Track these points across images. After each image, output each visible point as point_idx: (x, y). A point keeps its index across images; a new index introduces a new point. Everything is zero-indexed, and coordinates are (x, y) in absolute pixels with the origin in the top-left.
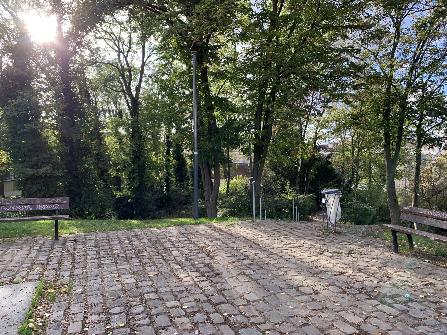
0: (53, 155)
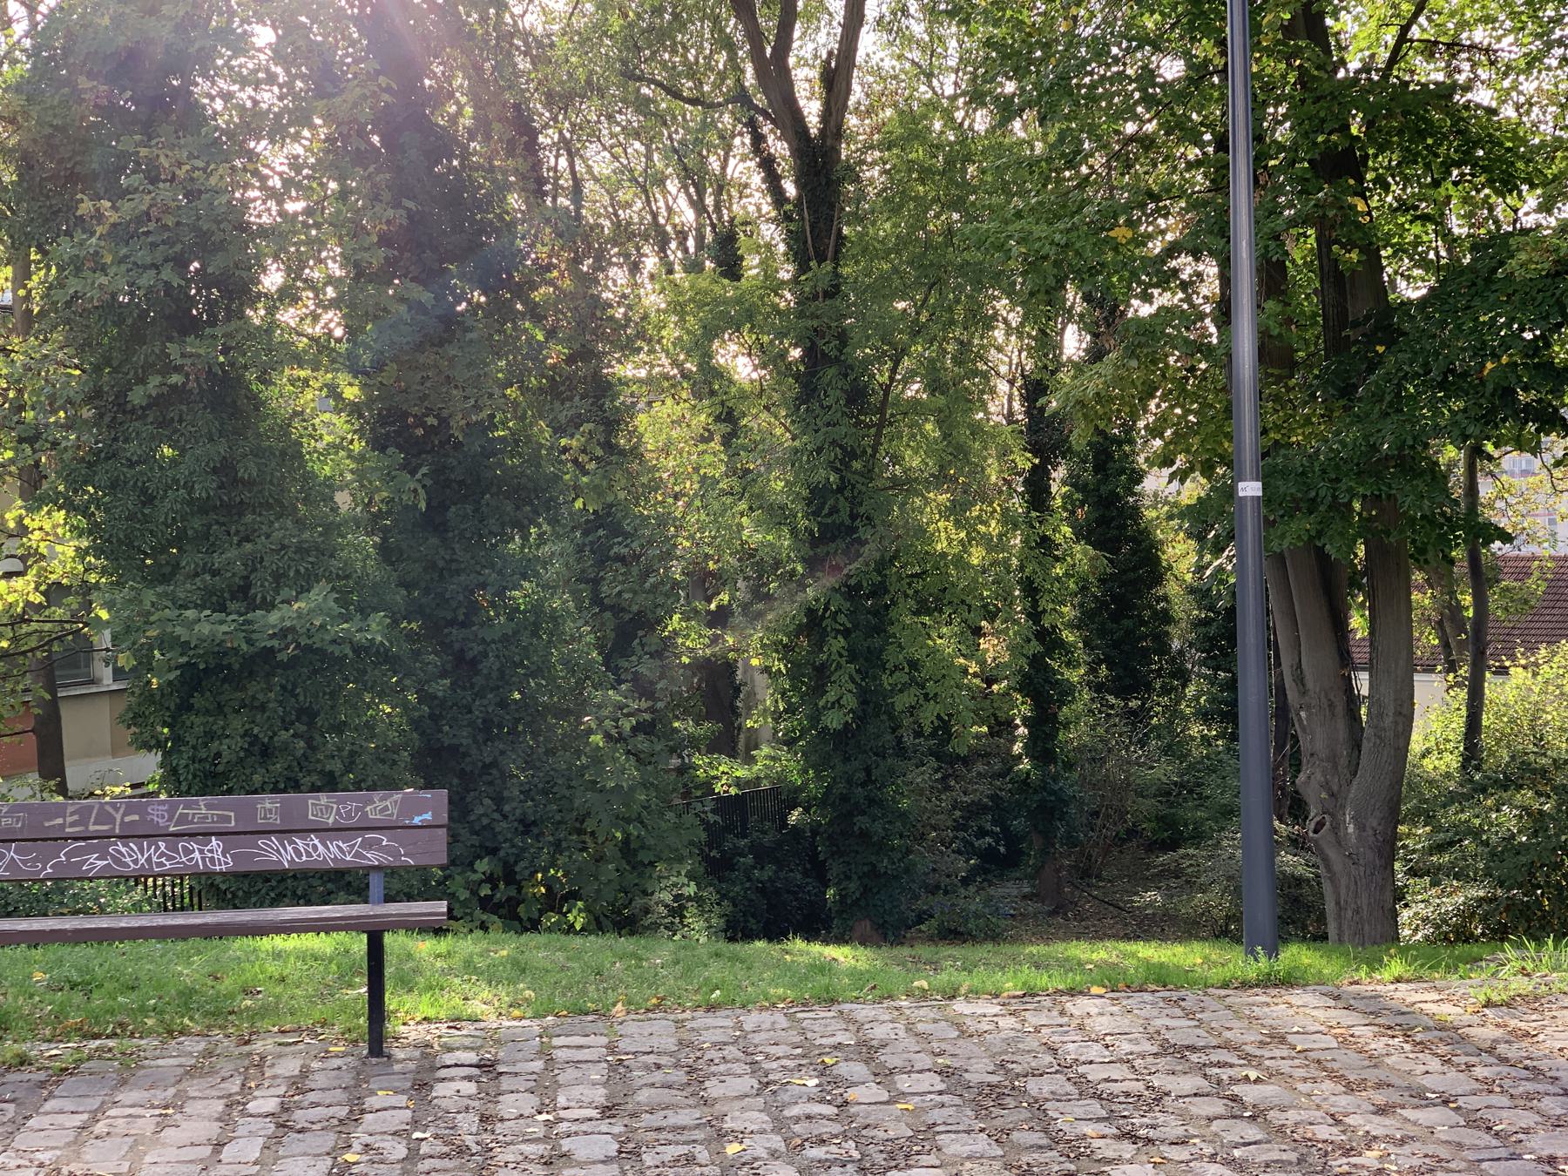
0: (330, 529)
